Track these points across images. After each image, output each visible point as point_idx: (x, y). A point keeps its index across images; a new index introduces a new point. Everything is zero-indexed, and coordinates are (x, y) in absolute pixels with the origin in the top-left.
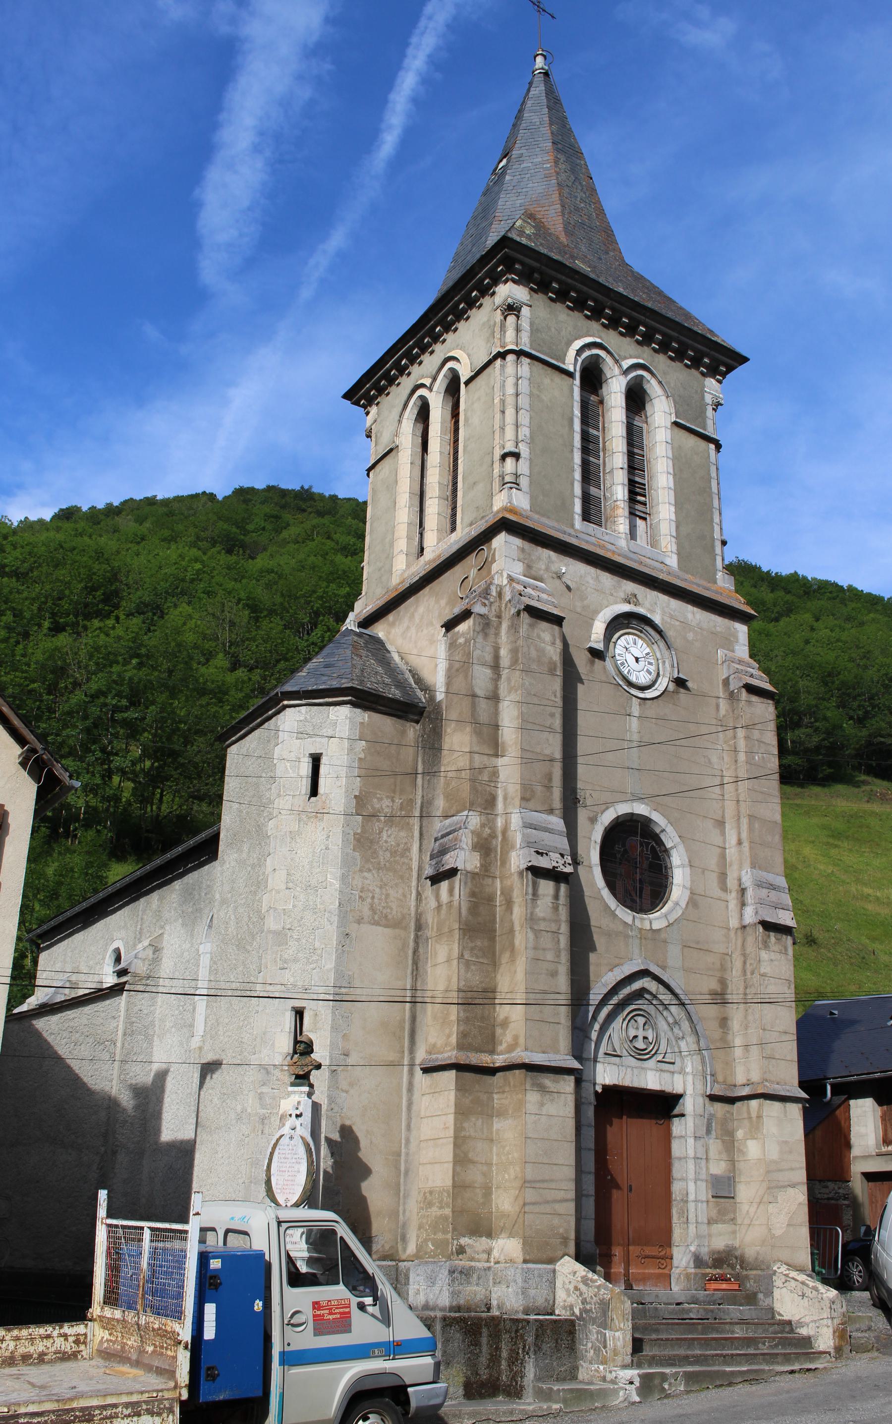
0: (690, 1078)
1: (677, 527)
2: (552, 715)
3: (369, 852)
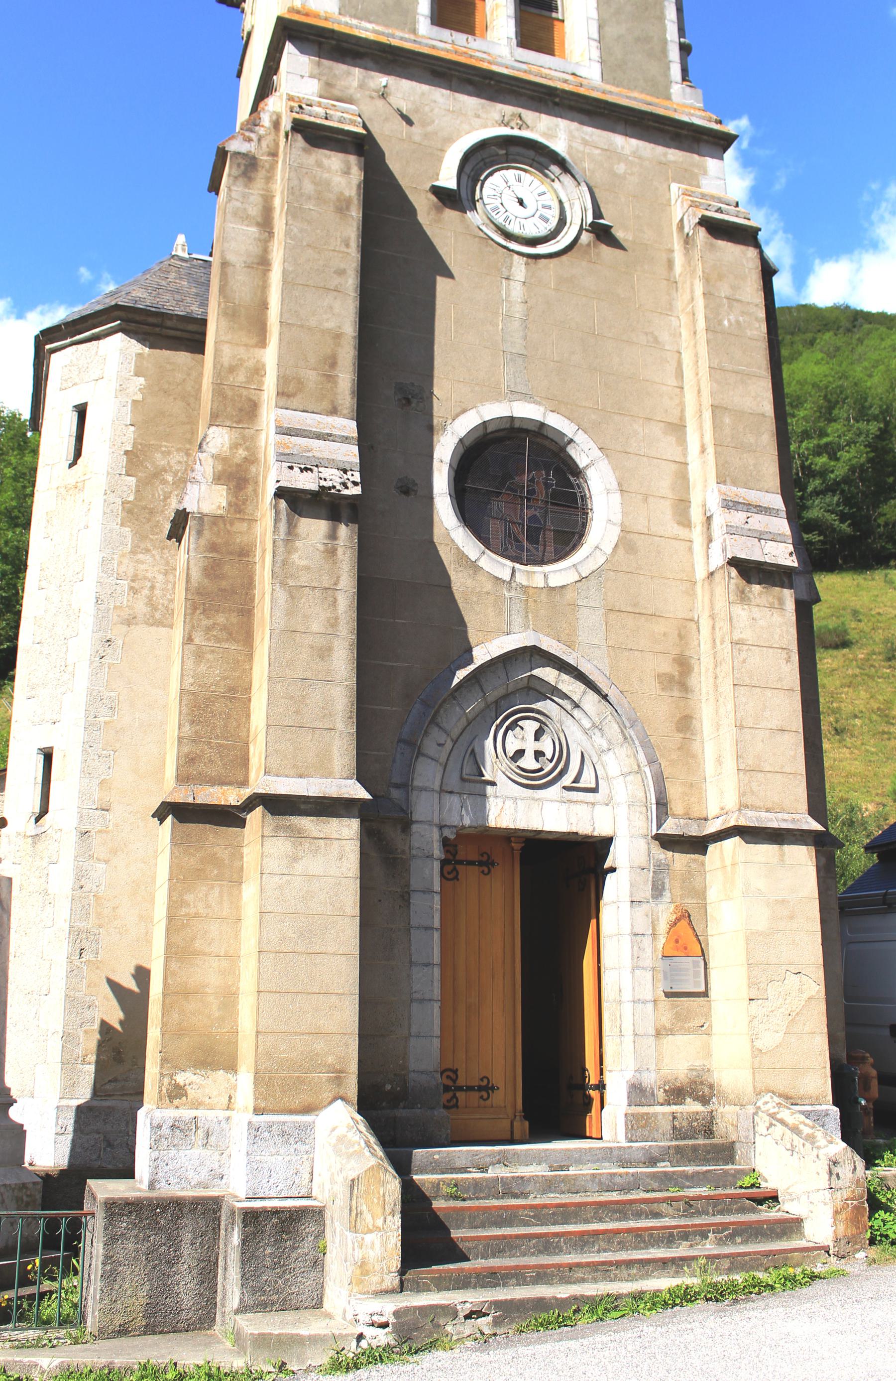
0: (622, 811)
1: (600, 27)
2: (341, 273)
3: (147, 526)
